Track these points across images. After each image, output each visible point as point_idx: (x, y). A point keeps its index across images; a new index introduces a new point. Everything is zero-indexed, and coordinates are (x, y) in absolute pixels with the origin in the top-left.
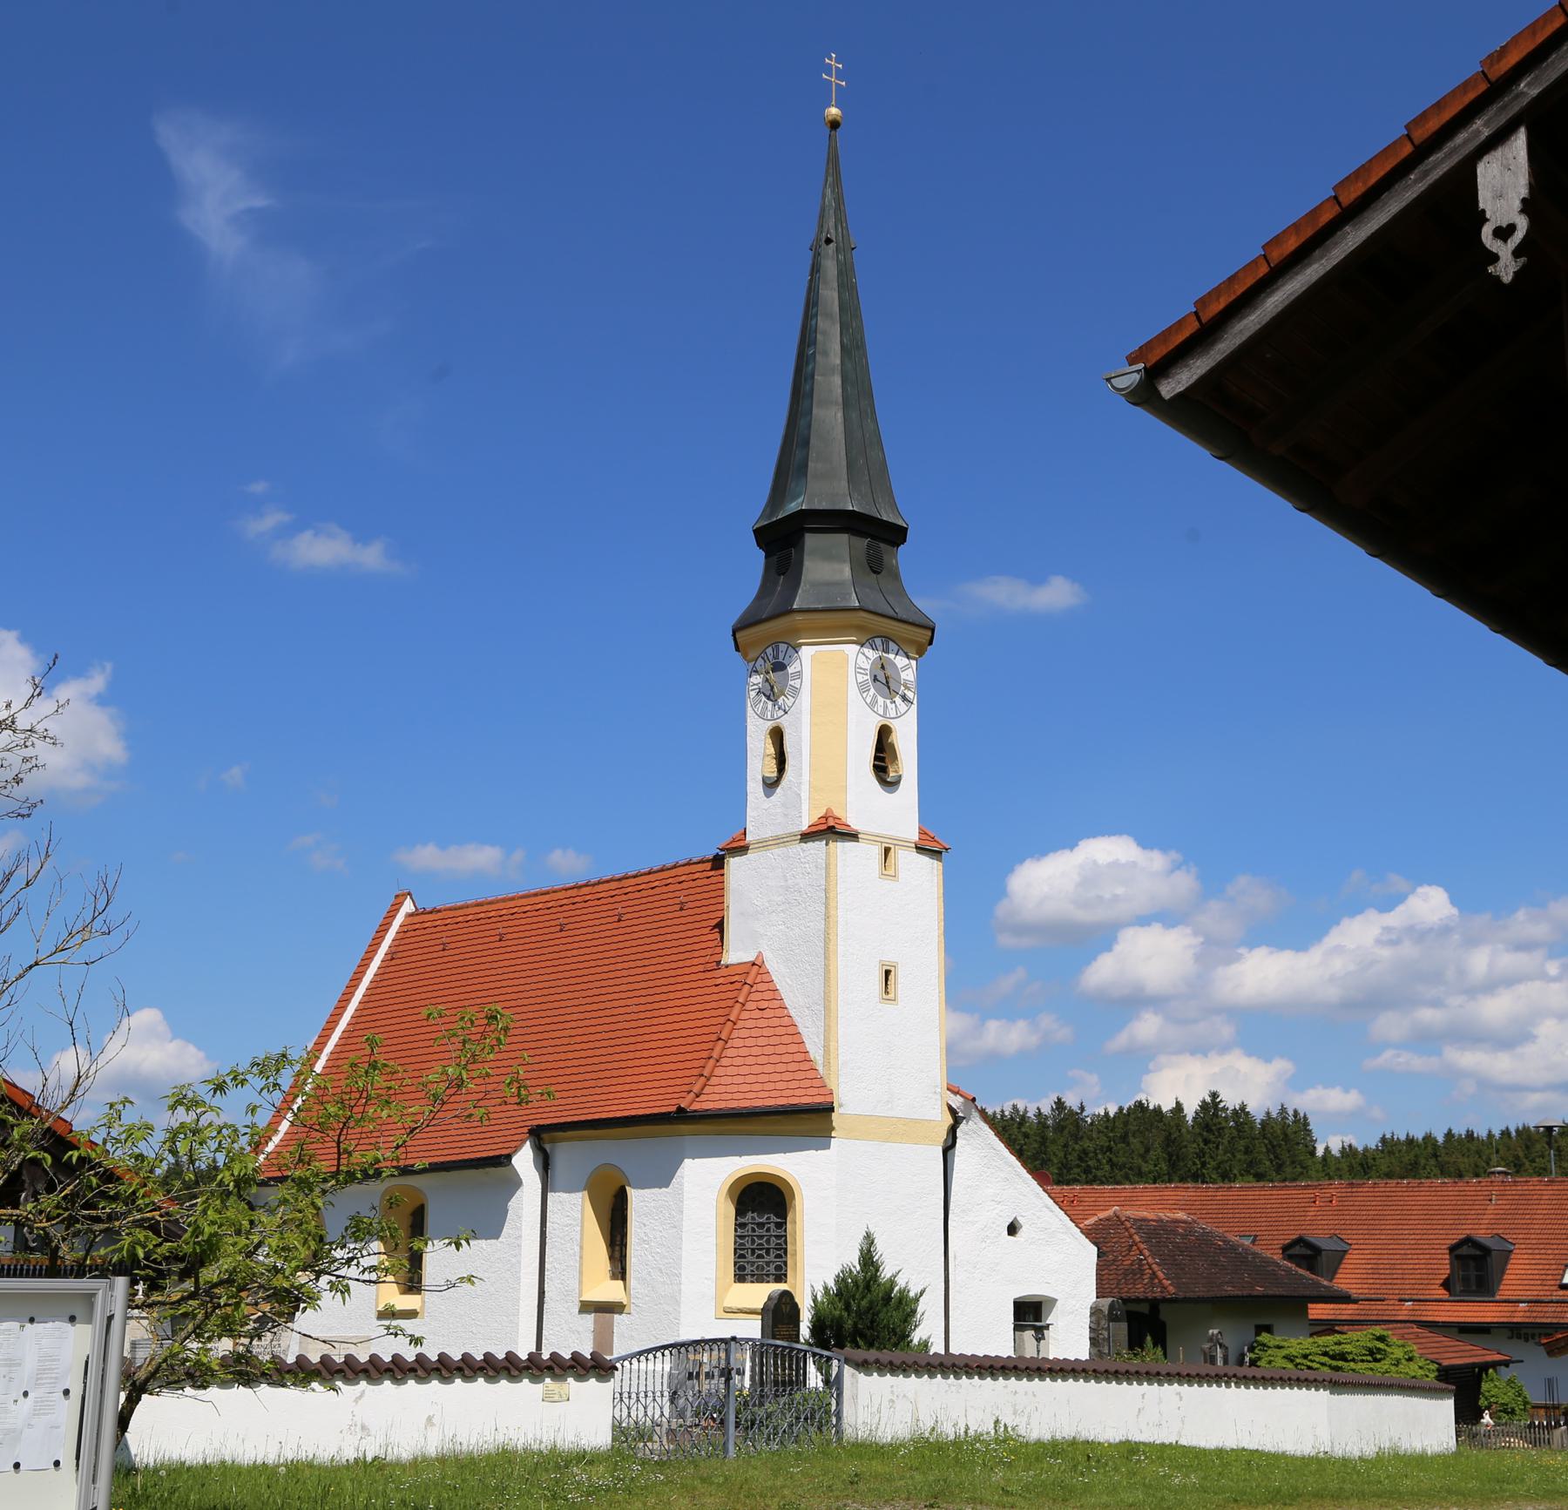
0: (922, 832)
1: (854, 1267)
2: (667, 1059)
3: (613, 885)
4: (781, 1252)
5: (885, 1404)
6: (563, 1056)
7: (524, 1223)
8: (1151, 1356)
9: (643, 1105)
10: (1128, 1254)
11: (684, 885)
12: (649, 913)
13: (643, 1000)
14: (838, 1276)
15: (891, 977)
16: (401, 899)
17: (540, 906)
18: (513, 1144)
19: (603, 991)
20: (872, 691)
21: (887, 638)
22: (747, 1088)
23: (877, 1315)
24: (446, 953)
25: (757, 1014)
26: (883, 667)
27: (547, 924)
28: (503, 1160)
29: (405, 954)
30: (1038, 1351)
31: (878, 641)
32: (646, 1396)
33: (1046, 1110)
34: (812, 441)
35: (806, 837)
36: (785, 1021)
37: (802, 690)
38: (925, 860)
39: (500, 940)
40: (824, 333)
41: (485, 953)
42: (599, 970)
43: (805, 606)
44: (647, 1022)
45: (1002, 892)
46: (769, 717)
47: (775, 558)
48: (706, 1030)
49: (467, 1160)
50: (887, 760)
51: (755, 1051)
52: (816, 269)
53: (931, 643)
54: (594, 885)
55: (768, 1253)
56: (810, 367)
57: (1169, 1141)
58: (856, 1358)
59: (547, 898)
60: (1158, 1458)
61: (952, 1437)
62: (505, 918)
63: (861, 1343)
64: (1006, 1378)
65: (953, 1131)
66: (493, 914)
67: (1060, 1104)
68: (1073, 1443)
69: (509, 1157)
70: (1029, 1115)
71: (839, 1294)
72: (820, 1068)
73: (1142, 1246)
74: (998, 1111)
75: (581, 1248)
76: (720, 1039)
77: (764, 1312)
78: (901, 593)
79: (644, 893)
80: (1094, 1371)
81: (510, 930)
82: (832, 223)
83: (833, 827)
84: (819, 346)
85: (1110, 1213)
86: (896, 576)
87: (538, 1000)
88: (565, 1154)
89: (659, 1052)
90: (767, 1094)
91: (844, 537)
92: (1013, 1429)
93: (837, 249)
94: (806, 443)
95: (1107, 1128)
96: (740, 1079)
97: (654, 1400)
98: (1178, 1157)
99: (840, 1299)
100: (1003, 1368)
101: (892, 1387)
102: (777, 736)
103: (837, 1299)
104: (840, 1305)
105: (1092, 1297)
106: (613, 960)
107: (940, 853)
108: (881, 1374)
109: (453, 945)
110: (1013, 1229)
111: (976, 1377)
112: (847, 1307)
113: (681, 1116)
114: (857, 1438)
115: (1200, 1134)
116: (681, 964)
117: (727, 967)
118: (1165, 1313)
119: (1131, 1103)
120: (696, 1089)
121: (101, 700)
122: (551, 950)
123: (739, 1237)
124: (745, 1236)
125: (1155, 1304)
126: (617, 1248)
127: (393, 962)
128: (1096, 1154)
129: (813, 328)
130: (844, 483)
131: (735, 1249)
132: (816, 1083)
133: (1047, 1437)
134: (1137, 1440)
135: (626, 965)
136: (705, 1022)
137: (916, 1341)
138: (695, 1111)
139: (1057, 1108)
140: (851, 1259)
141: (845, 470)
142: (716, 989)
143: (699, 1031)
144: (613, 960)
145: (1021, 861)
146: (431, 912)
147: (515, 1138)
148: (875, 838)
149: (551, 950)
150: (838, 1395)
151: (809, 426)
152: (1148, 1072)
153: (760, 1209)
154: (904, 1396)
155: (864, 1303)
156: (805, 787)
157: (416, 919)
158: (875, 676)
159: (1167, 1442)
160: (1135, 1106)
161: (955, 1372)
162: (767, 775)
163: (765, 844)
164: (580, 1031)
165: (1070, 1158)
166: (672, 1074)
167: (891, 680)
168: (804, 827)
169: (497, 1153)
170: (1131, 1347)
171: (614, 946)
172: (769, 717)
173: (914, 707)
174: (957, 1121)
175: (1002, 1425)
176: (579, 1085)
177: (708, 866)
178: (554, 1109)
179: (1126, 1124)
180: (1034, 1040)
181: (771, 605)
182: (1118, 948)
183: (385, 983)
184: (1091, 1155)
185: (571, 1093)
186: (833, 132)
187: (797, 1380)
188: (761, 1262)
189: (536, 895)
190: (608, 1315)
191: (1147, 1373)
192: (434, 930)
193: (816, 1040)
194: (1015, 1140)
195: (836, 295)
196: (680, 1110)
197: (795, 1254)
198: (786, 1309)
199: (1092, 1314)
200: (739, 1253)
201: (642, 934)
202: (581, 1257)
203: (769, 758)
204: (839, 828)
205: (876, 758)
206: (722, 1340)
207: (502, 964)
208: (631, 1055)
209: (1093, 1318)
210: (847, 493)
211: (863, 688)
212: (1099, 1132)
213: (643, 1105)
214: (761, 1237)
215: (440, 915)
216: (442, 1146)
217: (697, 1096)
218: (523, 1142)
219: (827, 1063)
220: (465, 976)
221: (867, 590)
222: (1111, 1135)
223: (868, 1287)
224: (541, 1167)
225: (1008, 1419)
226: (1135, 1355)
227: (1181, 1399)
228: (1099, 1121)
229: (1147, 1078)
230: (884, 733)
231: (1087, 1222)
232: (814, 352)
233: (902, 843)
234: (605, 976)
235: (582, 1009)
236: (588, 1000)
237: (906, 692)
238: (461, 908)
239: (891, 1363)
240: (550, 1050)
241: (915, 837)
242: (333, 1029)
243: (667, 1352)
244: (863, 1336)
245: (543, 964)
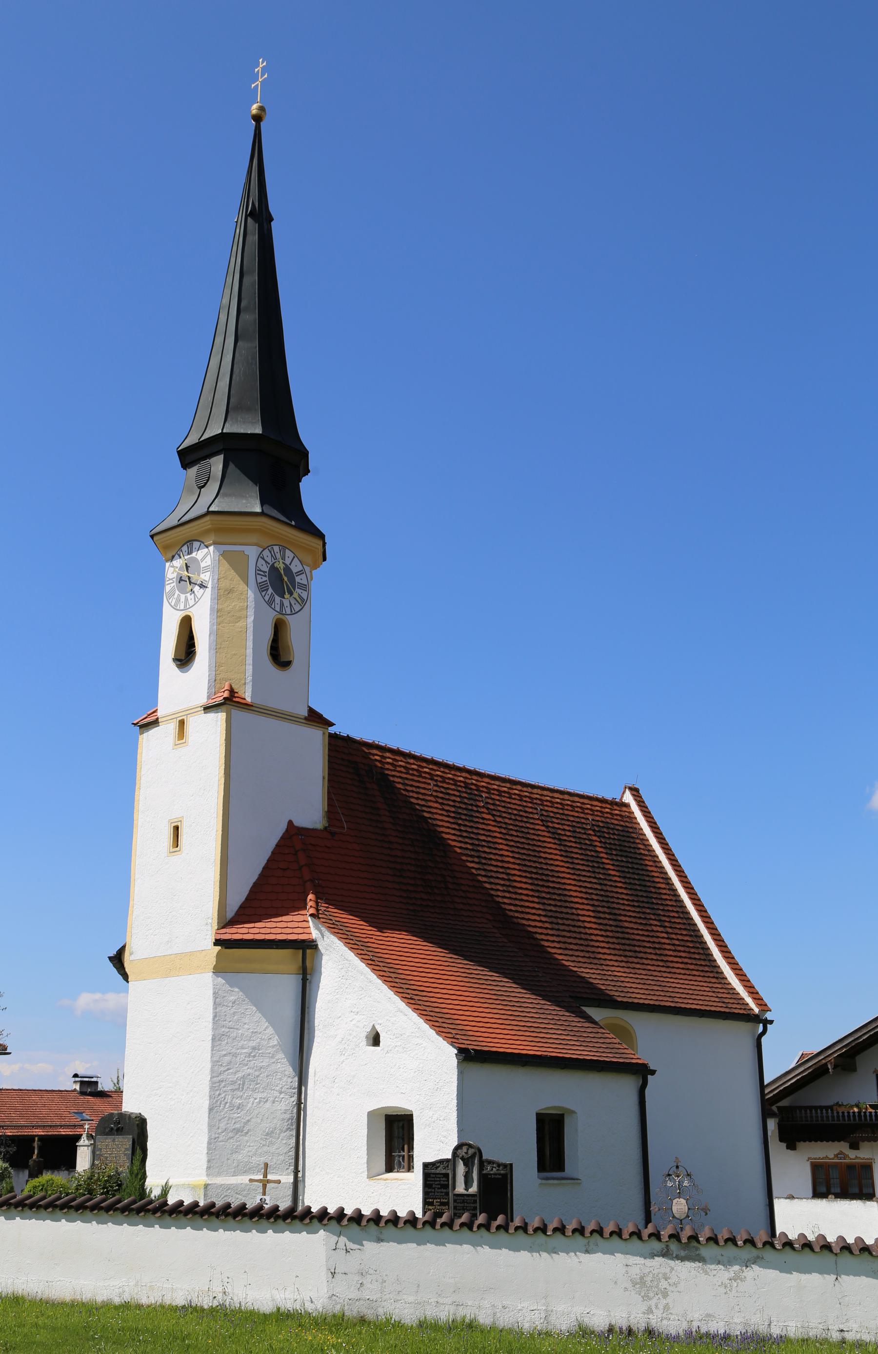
173: (209, 591)
205: (272, 647)
230: (186, 623)
233: (191, 711)
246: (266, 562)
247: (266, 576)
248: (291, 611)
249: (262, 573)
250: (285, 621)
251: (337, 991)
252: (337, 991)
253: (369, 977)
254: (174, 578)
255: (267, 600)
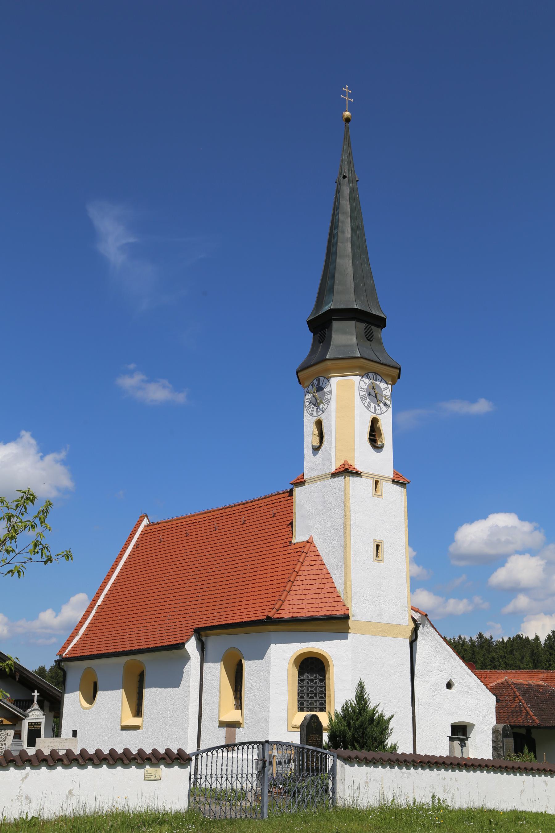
0: (395, 473)
1: (353, 701)
2: (263, 592)
3: (242, 506)
4: (323, 695)
5: (363, 784)
6: (213, 592)
7: (191, 680)
8: (527, 758)
9: (250, 616)
10: (513, 702)
11: (275, 505)
12: (258, 519)
13: (253, 563)
14: (343, 707)
15: (380, 548)
16: (142, 518)
17: (206, 519)
18: (186, 637)
19: (234, 559)
20: (368, 400)
21: (375, 373)
22: (303, 606)
23: (366, 729)
24: (162, 543)
25: (309, 568)
26: (373, 388)
27: (209, 527)
28: (180, 646)
29: (143, 545)
30: (462, 753)
31: (371, 375)
32: (212, 777)
33: (475, 638)
34: (336, 275)
35: (334, 475)
36: (324, 571)
37: (332, 400)
38: (397, 488)
39: (187, 536)
40: (343, 222)
41: (179, 543)
42: (232, 548)
43: (333, 357)
44: (255, 573)
45: (452, 539)
46: (315, 415)
47: (318, 335)
48: (283, 577)
49: (163, 646)
50: (376, 436)
51: (308, 587)
52: (338, 191)
53: (399, 377)
54: (232, 507)
55: (316, 696)
56: (335, 239)
57: (533, 654)
58: (344, 755)
59: (210, 514)
60: (535, 823)
61: (404, 806)
62: (190, 525)
63: (357, 746)
64: (439, 769)
65: (415, 631)
66: (184, 523)
67: (481, 636)
68: (481, 811)
69: (183, 644)
70: (466, 640)
71: (344, 717)
72: (342, 596)
73: (521, 698)
74: (452, 638)
75: (220, 692)
76: (290, 581)
77: (302, 726)
78: (383, 351)
79: (256, 510)
80: (493, 766)
81: (192, 531)
82: (346, 168)
83: (348, 469)
84: (340, 229)
85: (502, 680)
86: (380, 343)
87: (203, 565)
88: (212, 642)
89: (260, 588)
90: (314, 610)
91: (353, 323)
92: (444, 801)
93: (349, 181)
94: (333, 276)
95: (503, 647)
96: (300, 602)
97: (217, 780)
98: (538, 661)
99: (345, 720)
100: (436, 763)
101: (367, 773)
102: (319, 424)
103: (343, 720)
104: (345, 723)
105: (494, 723)
106: (239, 544)
107: (405, 484)
108: (360, 766)
109: (165, 540)
110: (449, 685)
111: (420, 768)
112: (349, 725)
113: (269, 621)
114: (345, 806)
115: (548, 651)
116: (272, 544)
117: (295, 544)
118: (535, 734)
119: (515, 636)
120: (277, 607)
121: (64, 463)
122: (210, 539)
123: (300, 686)
124: (304, 686)
125: (529, 729)
126: (239, 693)
127: (138, 549)
128: (499, 659)
129: (337, 220)
130: (353, 296)
131: (298, 693)
132: (340, 604)
133: (465, 807)
134: (521, 810)
135: (245, 546)
136: (283, 572)
137: (389, 745)
138: (276, 618)
139: (480, 638)
140: (351, 697)
141: (353, 289)
142: (289, 556)
143: (279, 577)
144: (239, 544)
145: (461, 525)
146: (156, 524)
147: (187, 634)
148: (370, 476)
149: (210, 539)
150: (333, 778)
151: (335, 268)
152: (523, 622)
153: (311, 671)
154: (375, 779)
155: (358, 723)
156: (333, 449)
157: (149, 528)
158: (369, 392)
159: (539, 811)
160: (516, 637)
161: (406, 765)
162: (314, 444)
163: (313, 480)
164: (222, 580)
165: (486, 661)
166: (265, 600)
167: (378, 395)
168: (333, 470)
169: (178, 642)
170: (516, 752)
171: (240, 537)
172: (315, 415)
173: (390, 409)
174: (417, 627)
175: (437, 799)
176: (220, 607)
177: (287, 494)
178: (207, 619)
179: (512, 645)
180: (470, 608)
181: (315, 359)
182: (508, 565)
183: (133, 559)
184: (496, 659)
185: (216, 611)
186: (347, 124)
187: (321, 767)
188: (312, 700)
189: (204, 513)
190: (233, 729)
191: (525, 768)
192: (157, 533)
193: (340, 581)
194: (460, 652)
195: (348, 203)
196: (268, 618)
197: (330, 696)
198: (314, 725)
199: (493, 733)
200: (300, 695)
201: (254, 530)
202: (220, 697)
203: (315, 436)
204: (351, 470)
205: (370, 435)
206: (260, 743)
207: (187, 548)
208: (246, 591)
209: (494, 735)
210: (354, 300)
211: (363, 398)
212: (500, 649)
213: (250, 616)
214: (312, 687)
215: (160, 526)
216: (153, 639)
217: (277, 611)
218: (191, 636)
219: (346, 593)
220: (170, 554)
221: (365, 349)
222: (505, 650)
223: (360, 713)
224: (200, 649)
225: (440, 795)
226: (518, 757)
227: (547, 785)
228: (499, 644)
229: (522, 625)
230: (374, 422)
231: (491, 685)
232: (337, 232)
233: (385, 479)
234: (235, 551)
235: (223, 568)
236: (227, 564)
237: (386, 401)
238: (170, 521)
239: (366, 758)
240: (207, 589)
241: (392, 476)
242: (107, 583)
243: (255, 746)
244: (358, 742)
245: (206, 547)
246: (365, 383)
247: (365, 391)
248: (381, 412)
249: (363, 390)
250: (377, 418)
251: (429, 657)
252: (429, 657)
253: (452, 653)
254: (310, 398)
255: (366, 406)
